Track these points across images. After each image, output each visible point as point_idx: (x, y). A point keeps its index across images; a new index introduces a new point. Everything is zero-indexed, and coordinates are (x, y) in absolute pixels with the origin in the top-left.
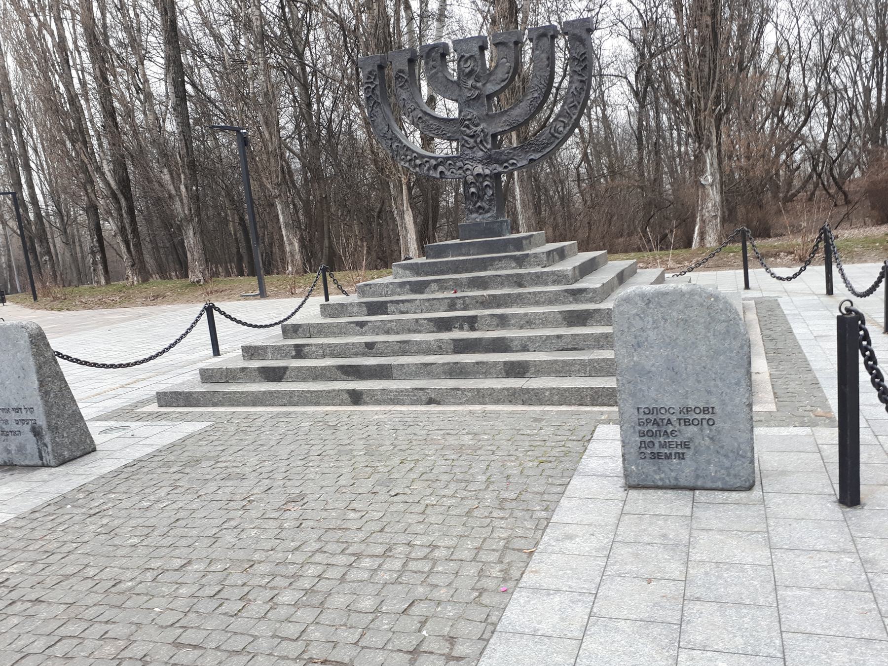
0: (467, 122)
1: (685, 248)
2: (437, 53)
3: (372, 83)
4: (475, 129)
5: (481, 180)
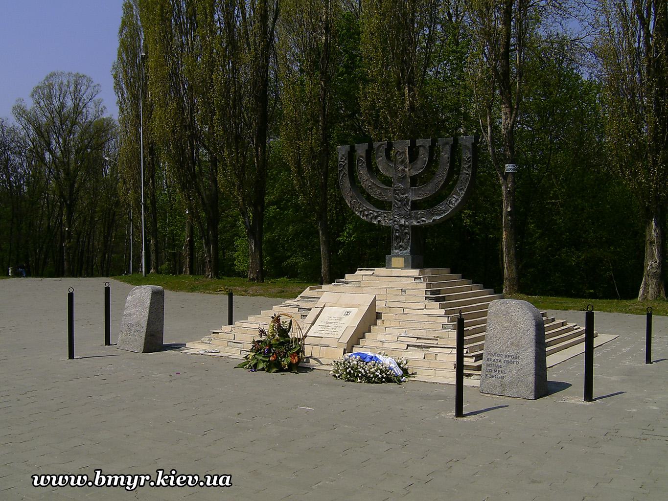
0: (397, 192)
1: (229, 325)
2: (383, 148)
3: (343, 162)
4: (402, 196)
5: (403, 228)
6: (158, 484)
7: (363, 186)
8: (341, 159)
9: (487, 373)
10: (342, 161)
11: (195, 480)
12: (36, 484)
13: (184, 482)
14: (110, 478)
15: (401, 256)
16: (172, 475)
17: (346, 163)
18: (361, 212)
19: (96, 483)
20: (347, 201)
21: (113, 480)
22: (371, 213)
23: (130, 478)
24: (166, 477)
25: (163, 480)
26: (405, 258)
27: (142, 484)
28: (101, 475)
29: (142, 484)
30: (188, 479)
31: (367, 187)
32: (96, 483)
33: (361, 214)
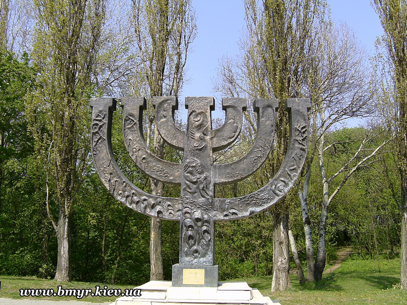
3: (100, 121)
5: (199, 224)
6: (96, 295)
7: (133, 158)
8: (97, 117)
10: (97, 120)
11: (119, 292)
12: (22, 294)
13: (112, 293)
14: (67, 291)
15: (199, 268)
16: (105, 289)
17: (105, 123)
18: (128, 197)
19: (59, 294)
20: (103, 180)
21: (69, 292)
22: (145, 200)
23: (79, 291)
24: (101, 291)
25: (99, 292)
26: (206, 271)
27: (86, 295)
28: (61, 289)
29: (86, 295)
30: (114, 292)
31: (139, 160)
32: (59, 294)
33: (126, 200)
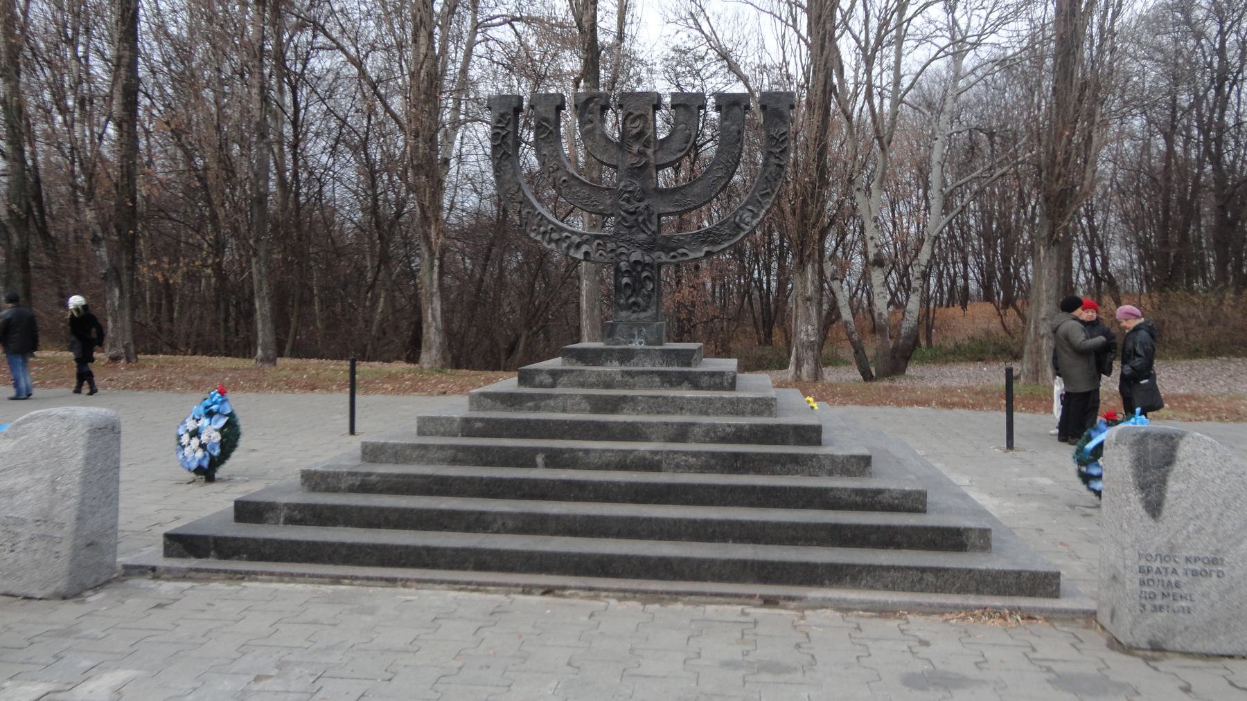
3: (502, 128)
9: (1143, 601)
18: (544, 233)
